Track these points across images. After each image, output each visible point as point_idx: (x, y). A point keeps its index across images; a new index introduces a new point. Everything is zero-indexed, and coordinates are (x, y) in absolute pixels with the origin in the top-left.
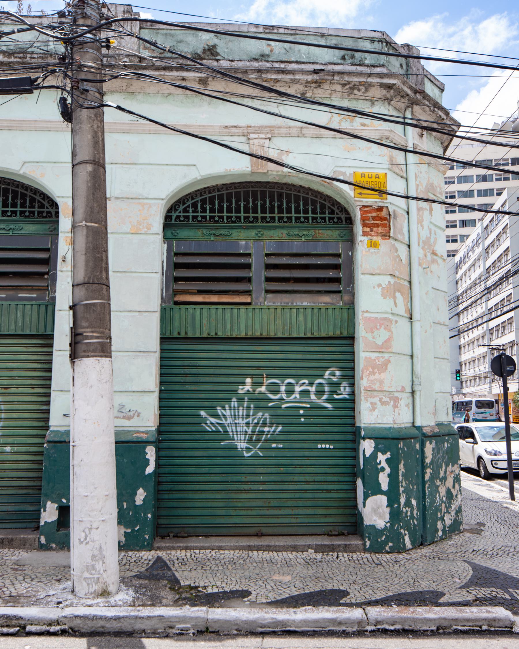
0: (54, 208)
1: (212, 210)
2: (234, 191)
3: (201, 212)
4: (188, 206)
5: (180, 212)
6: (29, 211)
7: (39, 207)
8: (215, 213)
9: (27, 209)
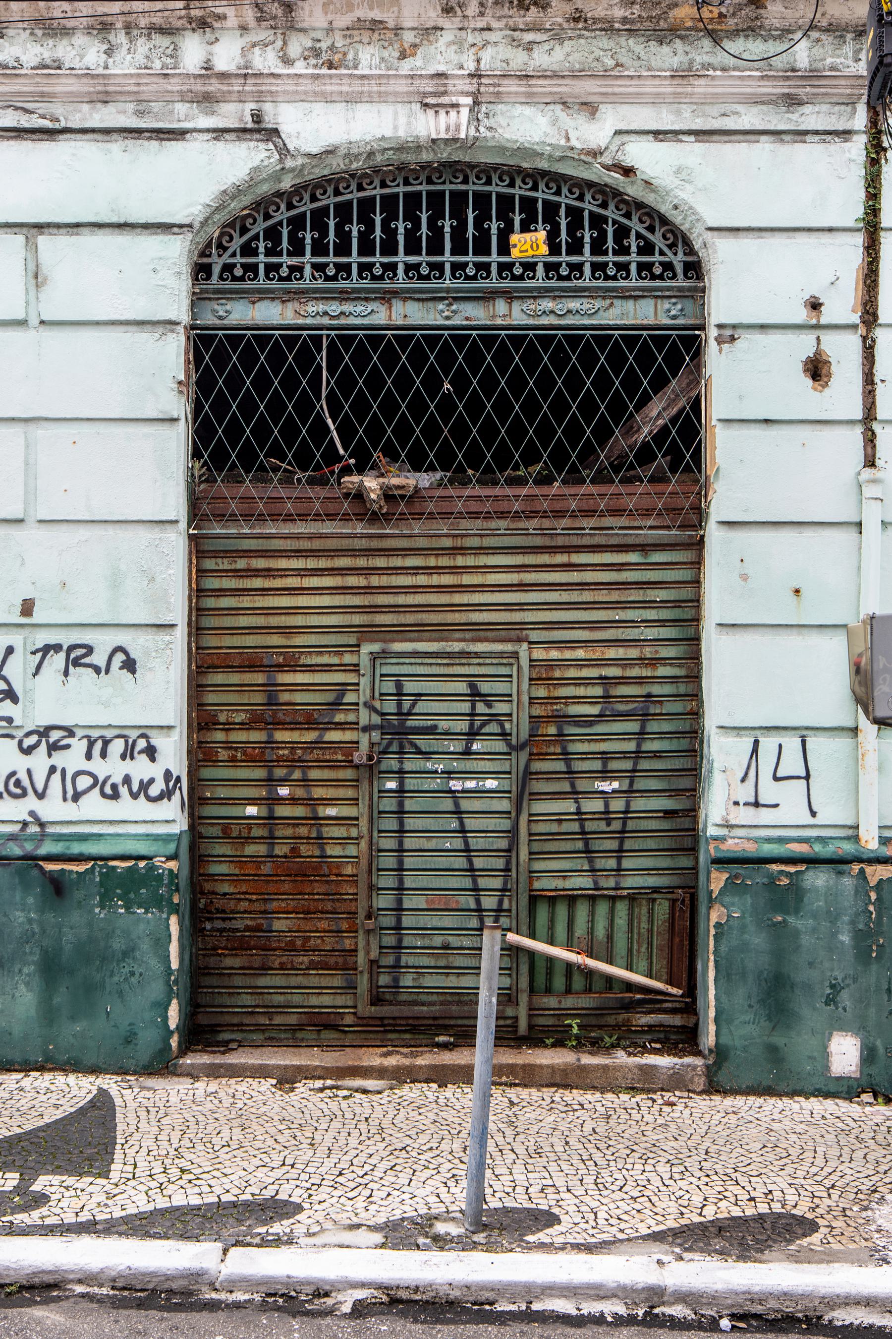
2: (402, 189)
4: (256, 237)
5: (234, 255)
8: (327, 254)
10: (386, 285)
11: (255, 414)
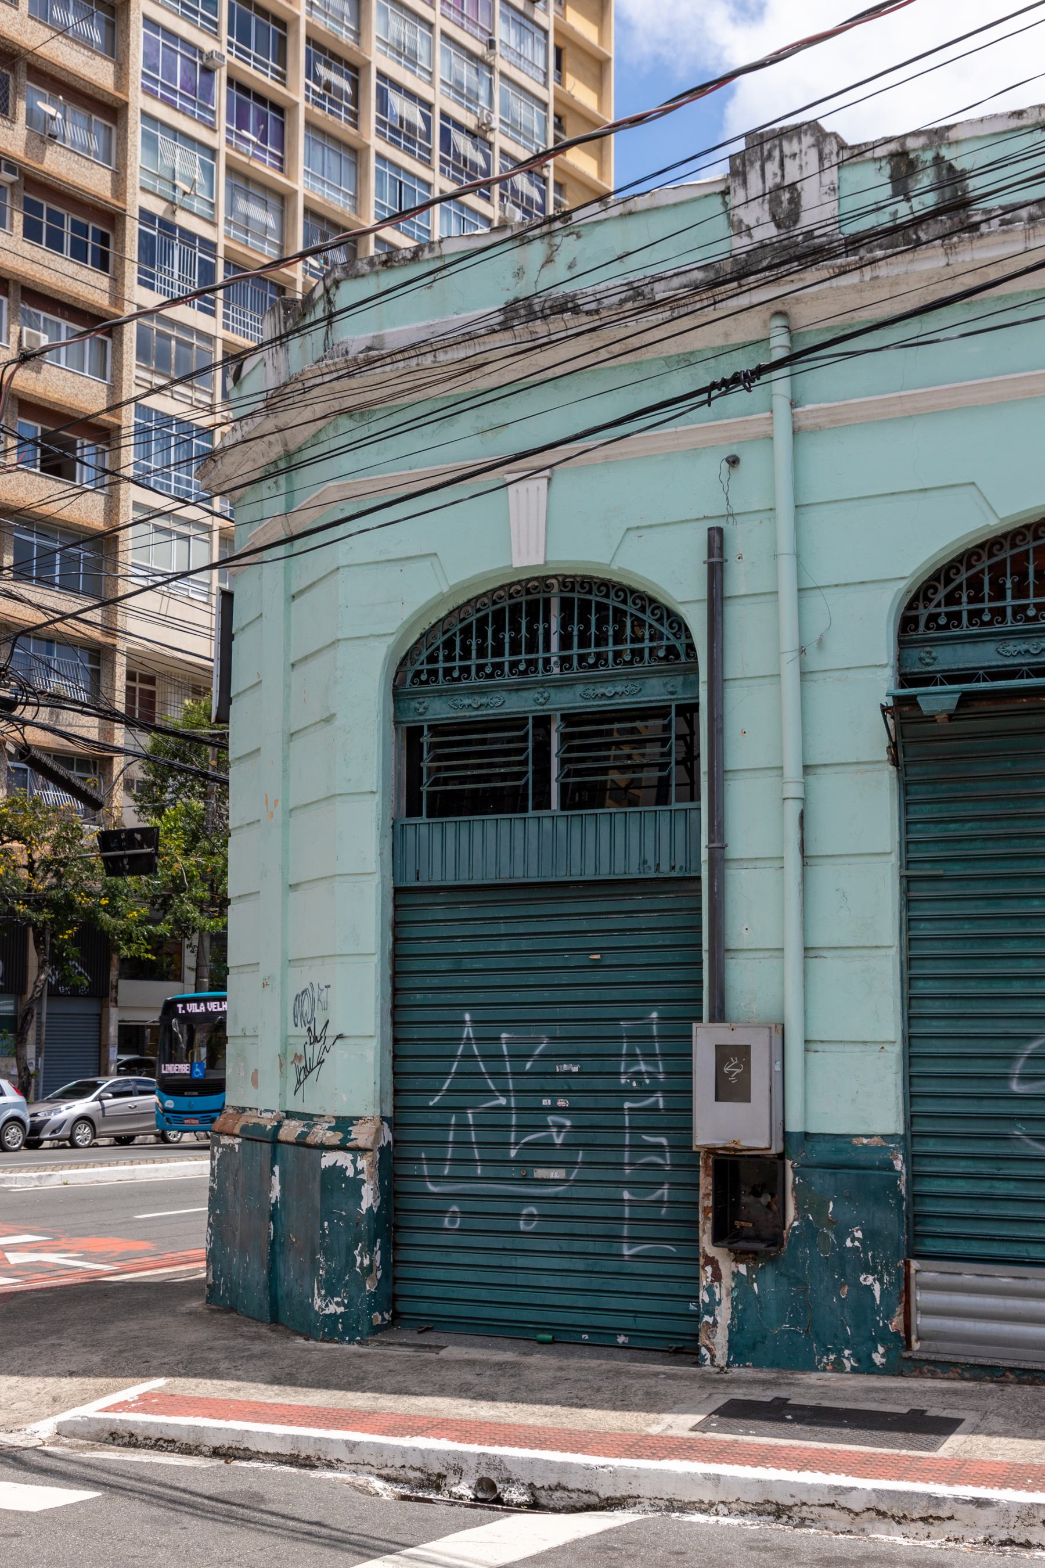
0: (683, 637)
3: (462, 658)
4: (959, 587)
5: (938, 605)
6: (991, 610)
8: (1028, 597)
10: (997, 628)
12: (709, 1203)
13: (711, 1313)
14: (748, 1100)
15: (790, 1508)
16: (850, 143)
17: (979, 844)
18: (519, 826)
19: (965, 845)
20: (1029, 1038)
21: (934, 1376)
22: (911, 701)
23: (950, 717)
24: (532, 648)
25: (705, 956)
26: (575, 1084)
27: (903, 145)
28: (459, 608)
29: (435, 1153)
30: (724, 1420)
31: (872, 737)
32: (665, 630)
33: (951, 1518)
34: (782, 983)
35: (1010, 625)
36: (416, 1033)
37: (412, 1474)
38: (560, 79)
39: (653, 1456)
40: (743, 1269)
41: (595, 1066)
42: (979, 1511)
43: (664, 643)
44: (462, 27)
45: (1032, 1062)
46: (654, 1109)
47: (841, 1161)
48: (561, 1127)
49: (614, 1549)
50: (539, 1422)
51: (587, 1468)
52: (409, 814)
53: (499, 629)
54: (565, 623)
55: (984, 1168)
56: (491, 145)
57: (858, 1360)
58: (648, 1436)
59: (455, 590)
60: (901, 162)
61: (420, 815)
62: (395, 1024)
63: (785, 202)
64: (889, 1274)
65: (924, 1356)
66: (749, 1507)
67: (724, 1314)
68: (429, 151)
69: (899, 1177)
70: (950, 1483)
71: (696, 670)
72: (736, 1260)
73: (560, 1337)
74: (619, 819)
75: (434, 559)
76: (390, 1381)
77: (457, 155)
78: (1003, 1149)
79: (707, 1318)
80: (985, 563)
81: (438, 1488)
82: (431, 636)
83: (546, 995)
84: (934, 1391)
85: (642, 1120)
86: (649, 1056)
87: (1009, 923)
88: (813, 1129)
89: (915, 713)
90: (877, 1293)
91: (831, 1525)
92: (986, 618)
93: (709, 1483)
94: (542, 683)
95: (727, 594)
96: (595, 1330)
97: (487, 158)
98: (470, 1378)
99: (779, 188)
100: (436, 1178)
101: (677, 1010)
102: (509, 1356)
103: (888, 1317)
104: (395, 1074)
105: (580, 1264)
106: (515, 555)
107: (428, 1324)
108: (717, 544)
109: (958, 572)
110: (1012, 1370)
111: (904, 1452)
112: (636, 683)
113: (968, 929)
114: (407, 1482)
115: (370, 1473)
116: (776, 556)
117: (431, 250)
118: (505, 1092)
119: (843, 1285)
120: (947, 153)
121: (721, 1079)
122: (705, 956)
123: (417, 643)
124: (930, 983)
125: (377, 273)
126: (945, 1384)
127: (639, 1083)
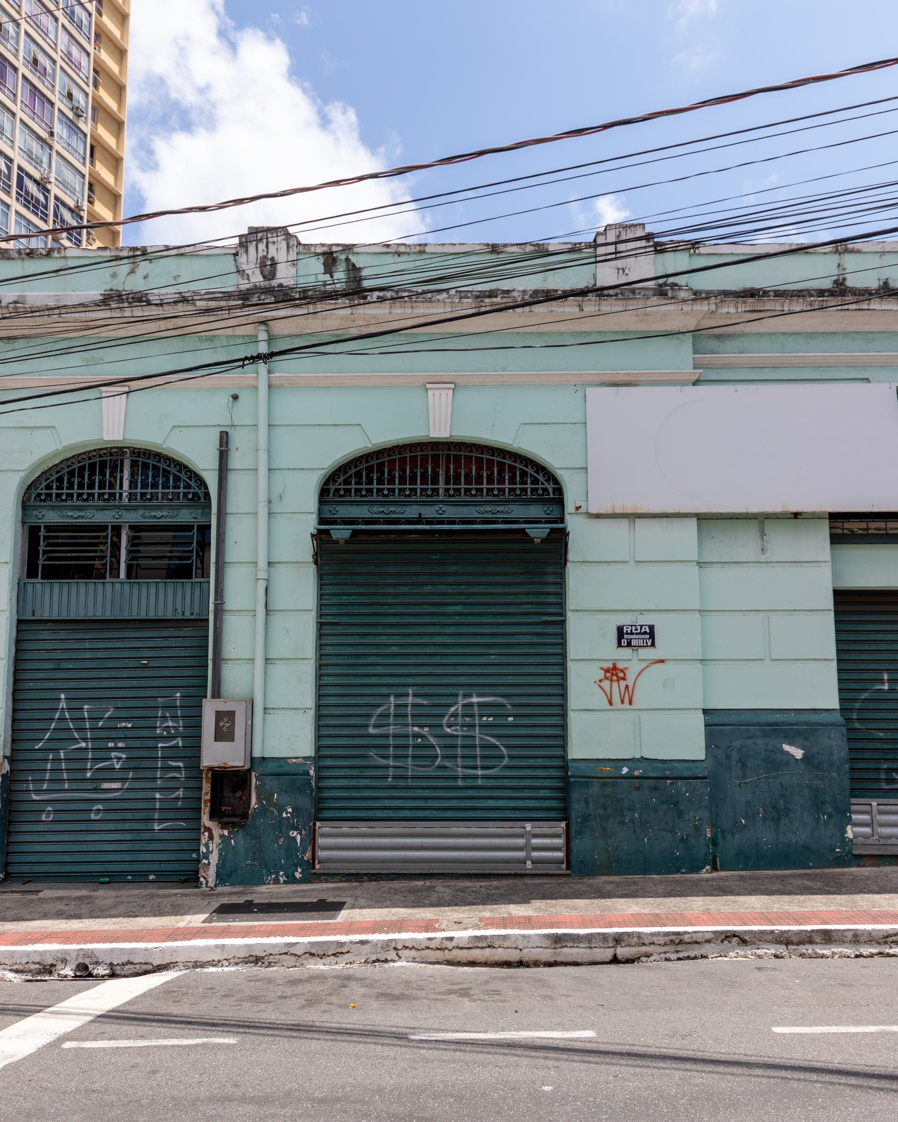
1: (81, 486)
3: (68, 488)
4: (351, 476)
5: (340, 484)
6: (366, 489)
7: (184, 488)
9: (364, 486)
10: (369, 499)
11: (50, 555)
12: (208, 797)
13: (207, 858)
14: (233, 741)
15: (263, 958)
16: (303, 242)
17: (357, 607)
18: (100, 587)
19: (350, 607)
20: (379, 706)
21: (327, 882)
22: (327, 532)
23: (347, 542)
24: (112, 486)
25: (210, 663)
26: (129, 734)
27: (330, 249)
28: (67, 459)
29: (38, 776)
30: (220, 915)
31: (305, 549)
32: (192, 484)
33: (348, 952)
34: (253, 677)
35: (375, 498)
36: (28, 705)
37: (33, 967)
38: (92, 163)
39: (184, 939)
40: (226, 832)
41: (142, 723)
42: (363, 947)
43: (192, 490)
44: (33, 119)
45: (380, 718)
46: (176, 747)
47: (282, 771)
48: (119, 758)
49: (173, 991)
50: (112, 928)
51: (146, 950)
52: (29, 577)
53: (92, 474)
54: (132, 475)
55: (355, 772)
56: (48, 191)
57: (287, 877)
58: (178, 929)
59: (66, 449)
60: (328, 257)
61: (37, 577)
62: (14, 700)
63: (269, 267)
64: (305, 830)
65: (322, 871)
66: (240, 960)
67: (214, 858)
68: (9, 187)
69: (311, 779)
70: (347, 934)
71: (210, 507)
72: (222, 828)
73: (114, 879)
74: (161, 586)
75: (53, 430)
76: (9, 914)
77: (27, 193)
78: (364, 763)
79: (205, 861)
80: (364, 465)
81: (50, 973)
82: (48, 474)
83: (113, 684)
84: (328, 889)
85: (168, 753)
86: (174, 717)
87: (371, 647)
88: (266, 756)
89: (328, 539)
90: (299, 841)
91: (285, 964)
92: (364, 493)
93: (218, 950)
94: (118, 507)
95: (229, 467)
96: (135, 873)
97: (46, 198)
98: (61, 907)
99: (265, 257)
100: (37, 792)
101: (193, 692)
102: (84, 893)
103: (304, 852)
104: (13, 730)
105: (128, 836)
106: (105, 432)
107: (29, 878)
108: (225, 440)
109: (350, 468)
110: (366, 875)
111: (320, 921)
112: (175, 511)
113: (350, 650)
114: (30, 971)
115: (4, 969)
116: (257, 450)
117: (59, 252)
118: (85, 739)
119: (280, 837)
120: (353, 259)
121: (218, 729)
122: (210, 663)
123: (39, 477)
124: (330, 678)
125: (23, 259)
126: (333, 885)
127: (168, 733)
